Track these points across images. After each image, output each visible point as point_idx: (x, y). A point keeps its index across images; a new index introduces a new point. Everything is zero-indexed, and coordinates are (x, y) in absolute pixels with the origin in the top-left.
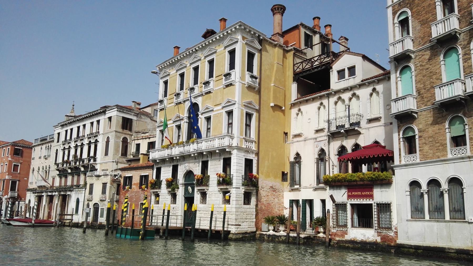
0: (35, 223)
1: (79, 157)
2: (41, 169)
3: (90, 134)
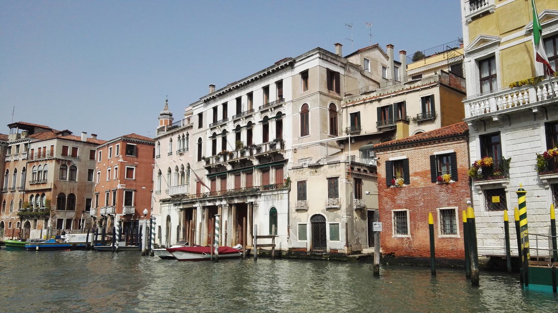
0: (219, 253)
1: (245, 144)
2: (173, 171)
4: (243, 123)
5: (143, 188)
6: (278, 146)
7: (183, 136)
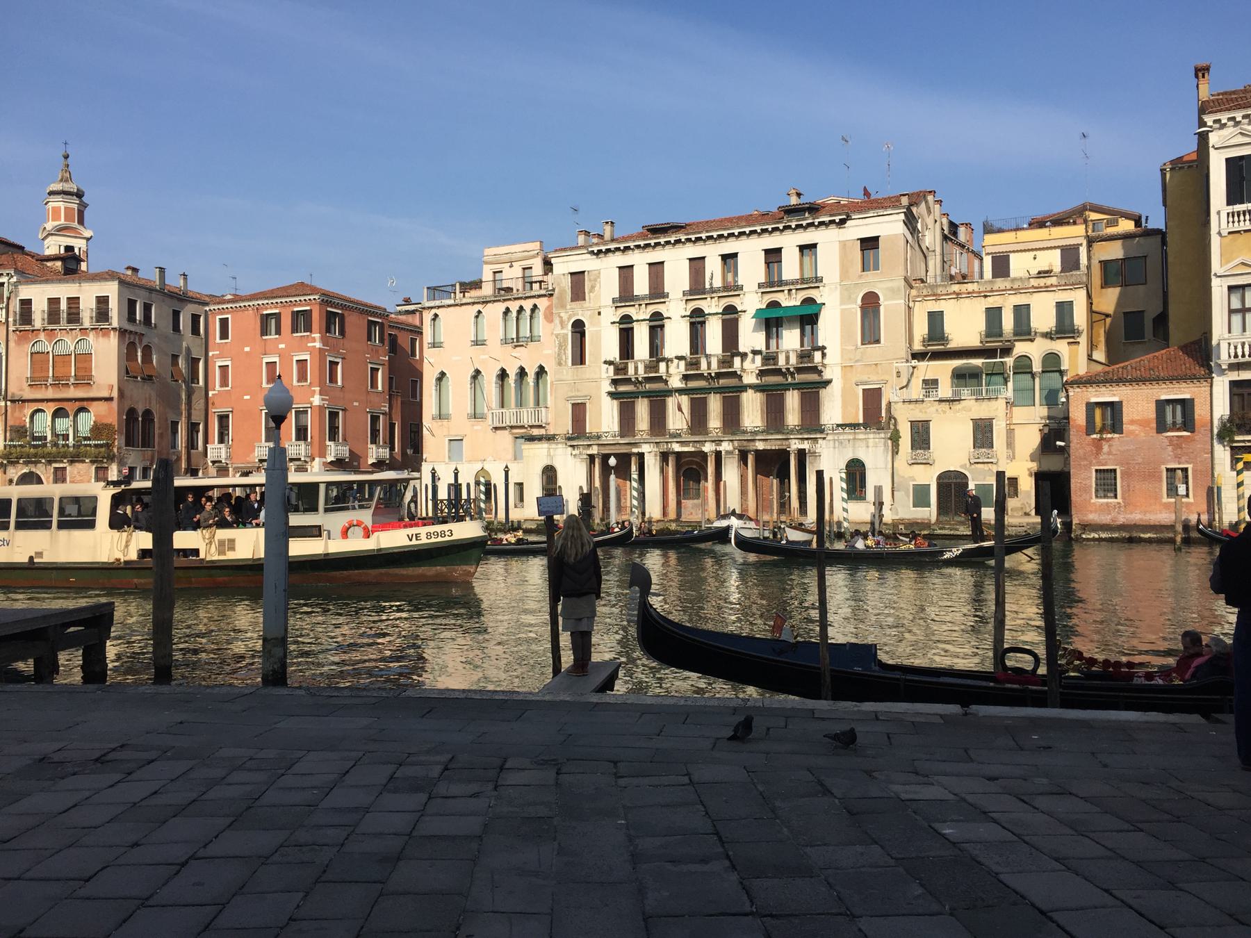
4: (712, 306)
7: (521, 309)
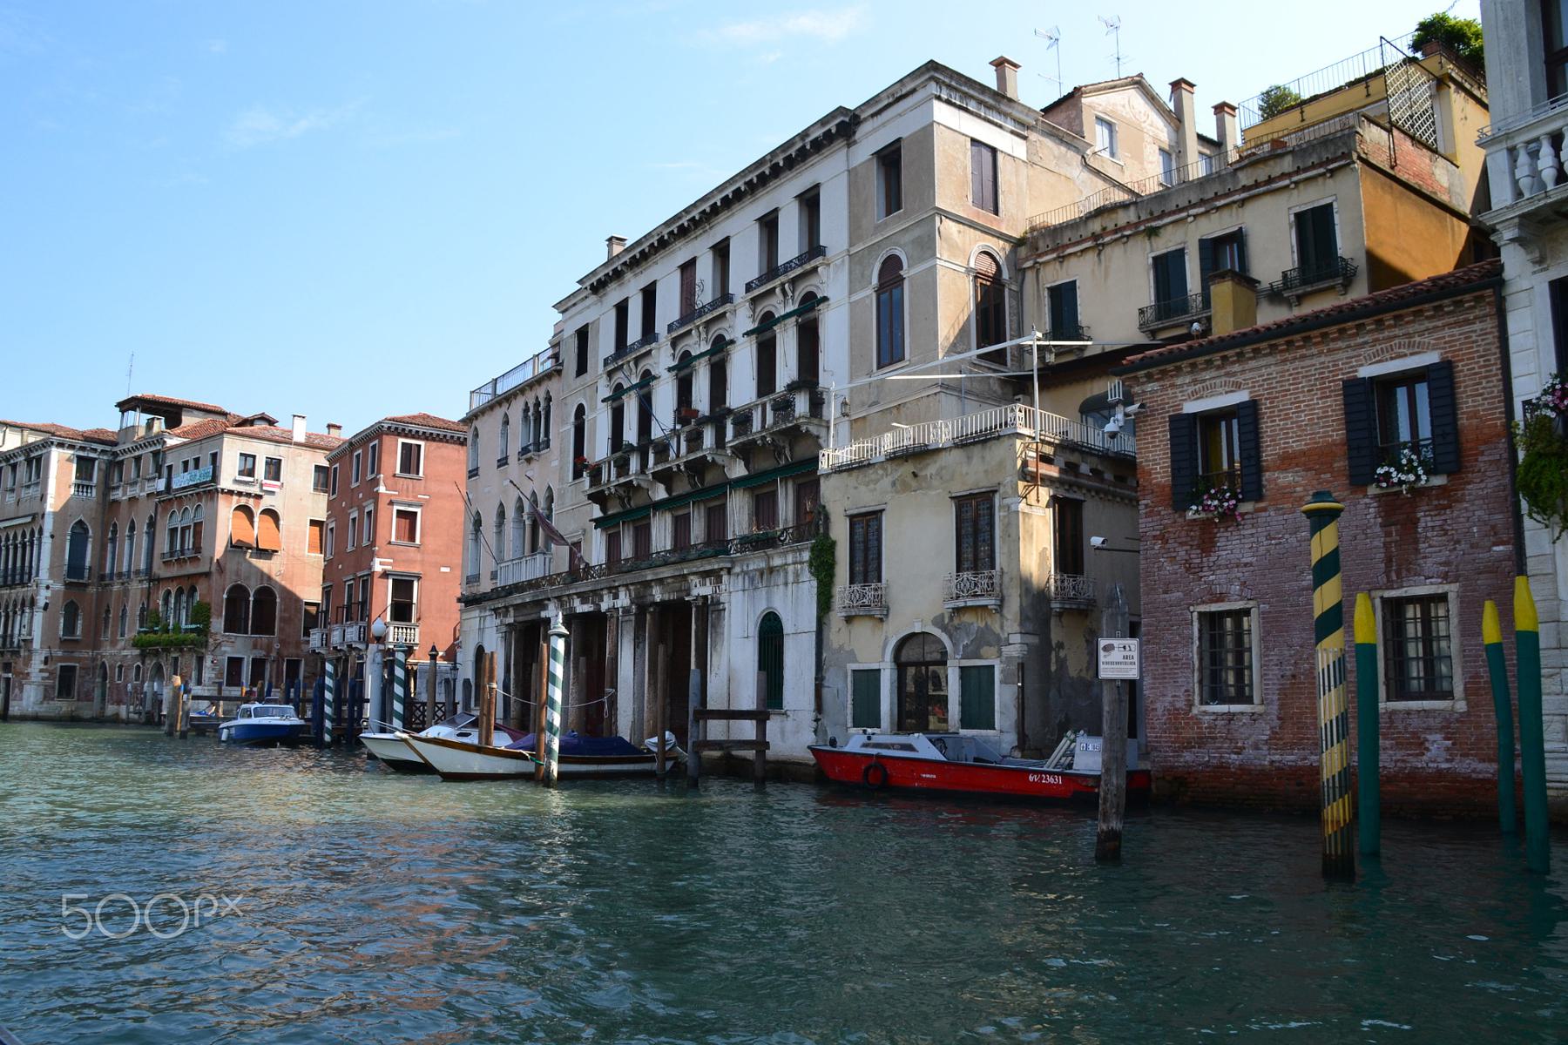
2: (510, 513)
3: (762, 280)
4: (698, 345)
5: (443, 570)
6: (801, 404)
7: (537, 404)
